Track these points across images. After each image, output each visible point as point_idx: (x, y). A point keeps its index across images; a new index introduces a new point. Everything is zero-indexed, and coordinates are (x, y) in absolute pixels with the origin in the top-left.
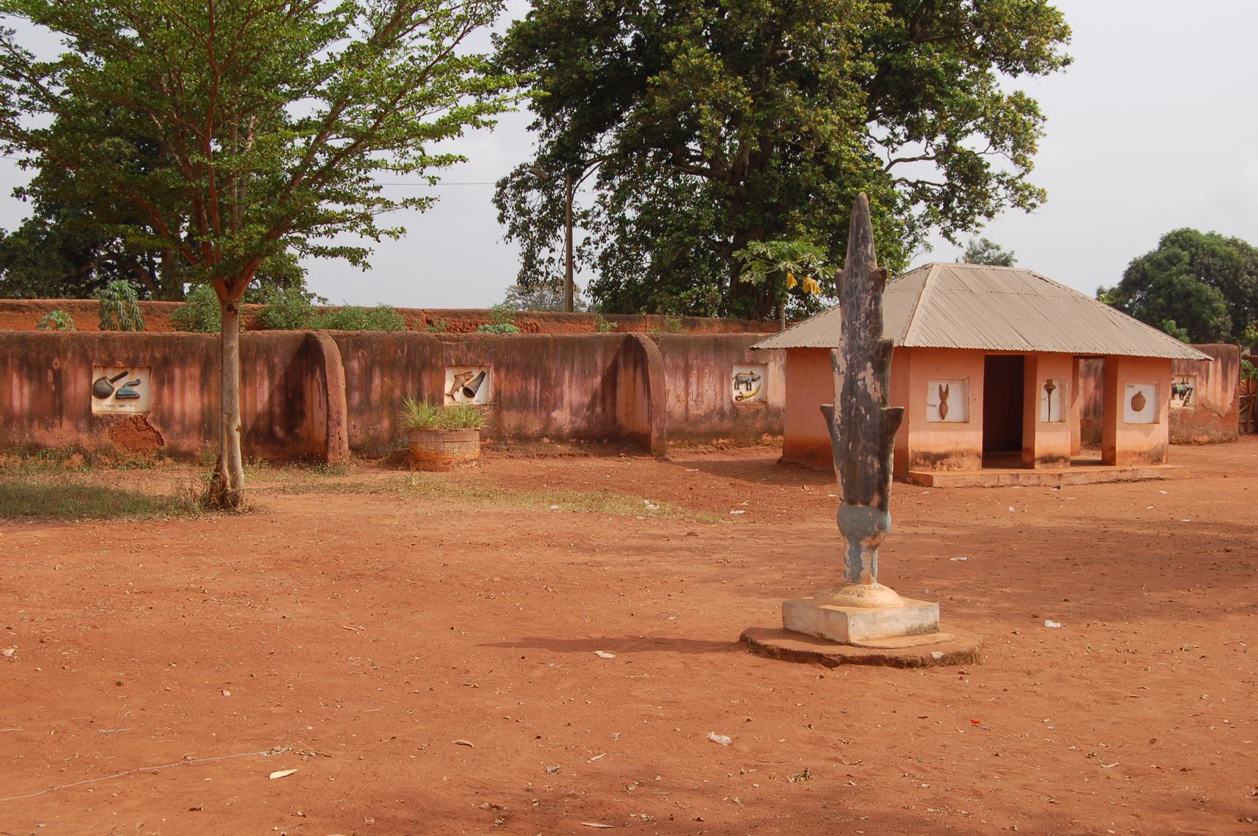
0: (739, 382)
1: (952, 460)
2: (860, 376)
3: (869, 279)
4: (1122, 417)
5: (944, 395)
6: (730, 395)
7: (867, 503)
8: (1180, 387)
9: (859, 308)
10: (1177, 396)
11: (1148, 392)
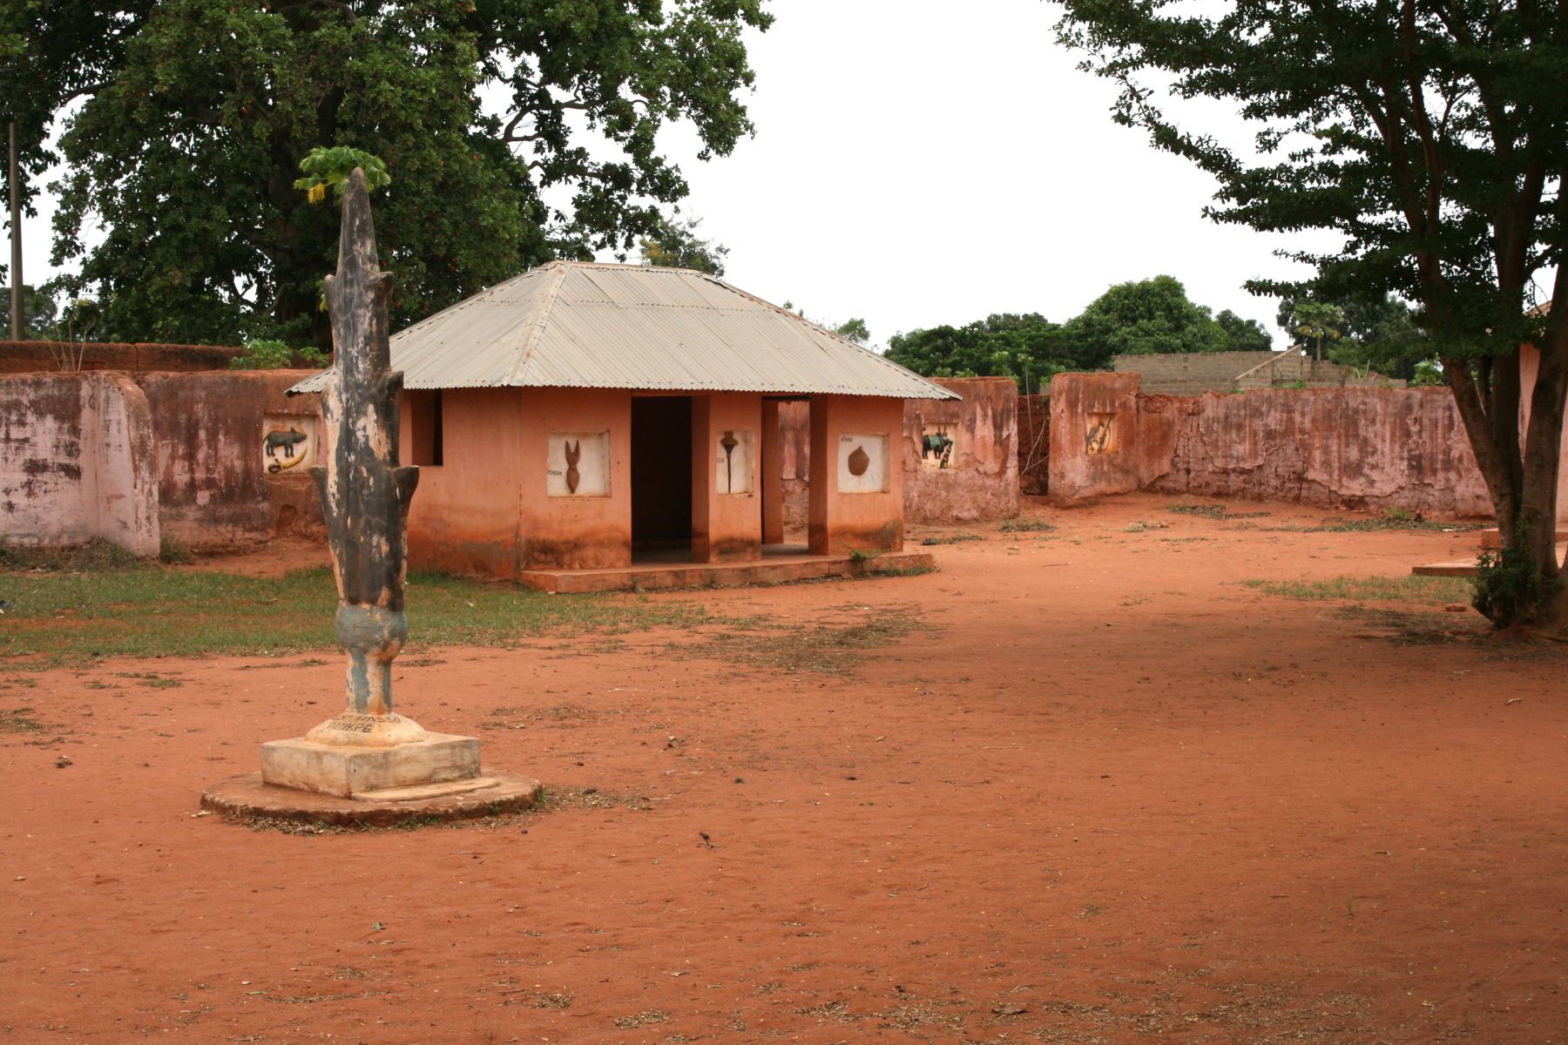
0: (274, 443)
1: (589, 552)
2: (360, 424)
3: (368, 288)
4: (836, 485)
5: (573, 457)
6: (260, 461)
7: (373, 601)
8: (935, 441)
9: (356, 330)
10: (931, 454)
11: (873, 448)
